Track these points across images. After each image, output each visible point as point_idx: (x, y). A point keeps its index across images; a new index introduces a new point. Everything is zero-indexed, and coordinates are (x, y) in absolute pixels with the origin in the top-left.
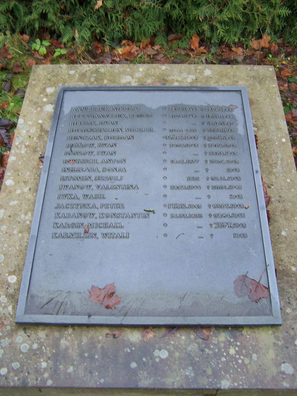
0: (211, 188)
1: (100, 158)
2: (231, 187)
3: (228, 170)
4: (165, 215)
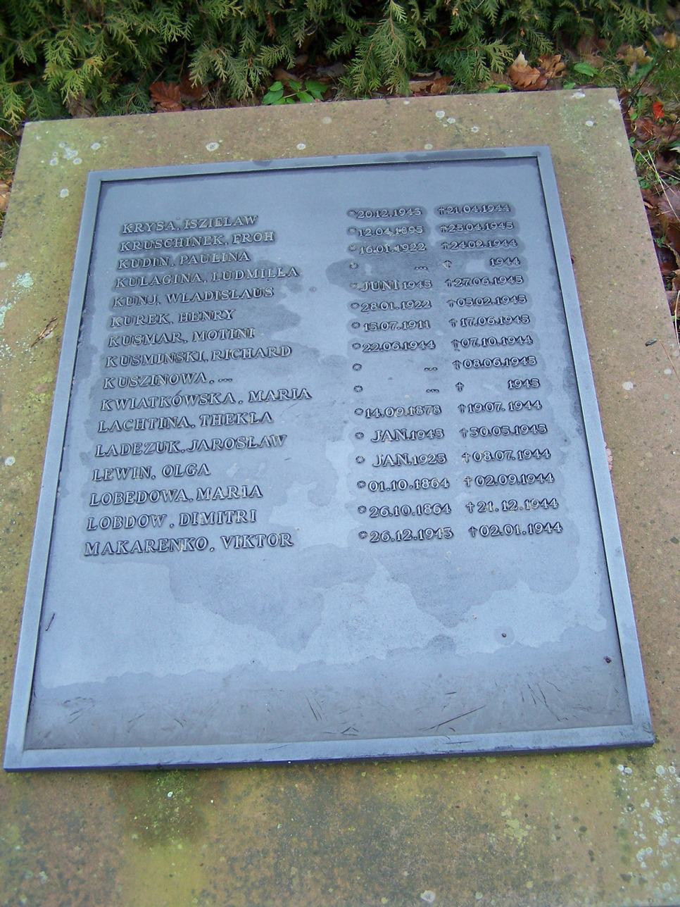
2: (508, 363)
3: (513, 385)
4: (360, 435)
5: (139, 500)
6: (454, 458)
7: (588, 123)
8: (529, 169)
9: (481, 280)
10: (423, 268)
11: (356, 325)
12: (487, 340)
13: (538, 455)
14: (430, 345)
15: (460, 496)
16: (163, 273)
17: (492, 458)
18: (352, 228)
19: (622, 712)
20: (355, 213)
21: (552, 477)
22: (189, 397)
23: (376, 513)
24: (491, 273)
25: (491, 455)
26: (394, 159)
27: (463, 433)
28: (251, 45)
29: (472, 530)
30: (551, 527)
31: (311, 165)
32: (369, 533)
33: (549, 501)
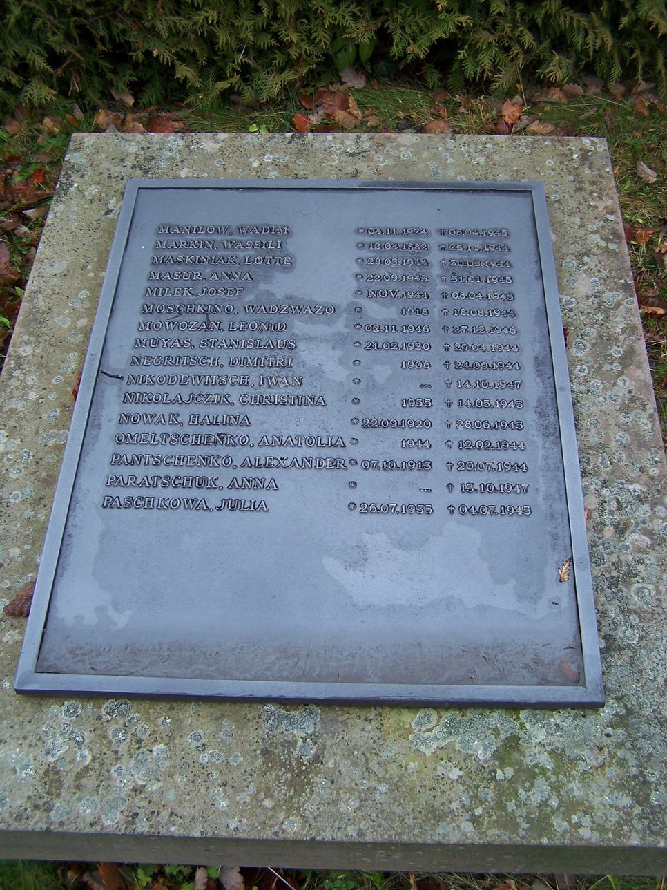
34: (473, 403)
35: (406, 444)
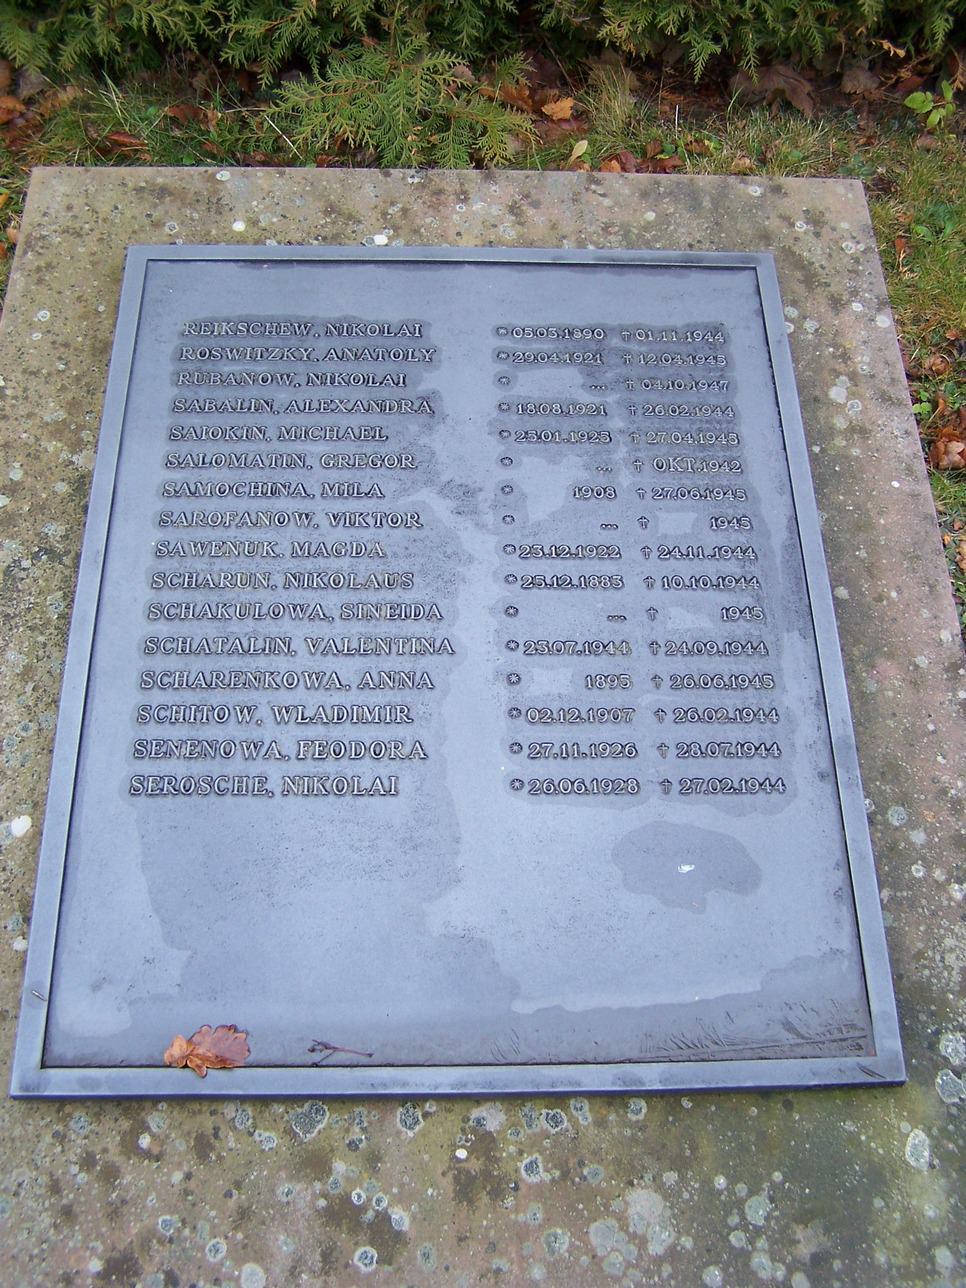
0: (655, 554)
1: (289, 737)
5: (252, 649)
6: (647, 752)
7: (832, 210)
8: (752, 272)
9: (689, 492)
10: (596, 387)
11: (512, 645)
12: (697, 581)
13: (762, 717)
14: (615, 583)
15: (646, 699)
16: (260, 369)
17: (702, 753)
18: (502, 328)
19: (860, 1041)
20: (505, 331)
21: (778, 749)
22: (300, 516)
23: (538, 752)
24: (712, 539)
25: (700, 749)
26: (561, 258)
27: (649, 582)
28: (134, 1244)
29: (666, 784)
30: (766, 749)
31: (443, 257)
32: (526, 782)
33: (773, 783)
34: (690, 646)
35: (591, 682)
